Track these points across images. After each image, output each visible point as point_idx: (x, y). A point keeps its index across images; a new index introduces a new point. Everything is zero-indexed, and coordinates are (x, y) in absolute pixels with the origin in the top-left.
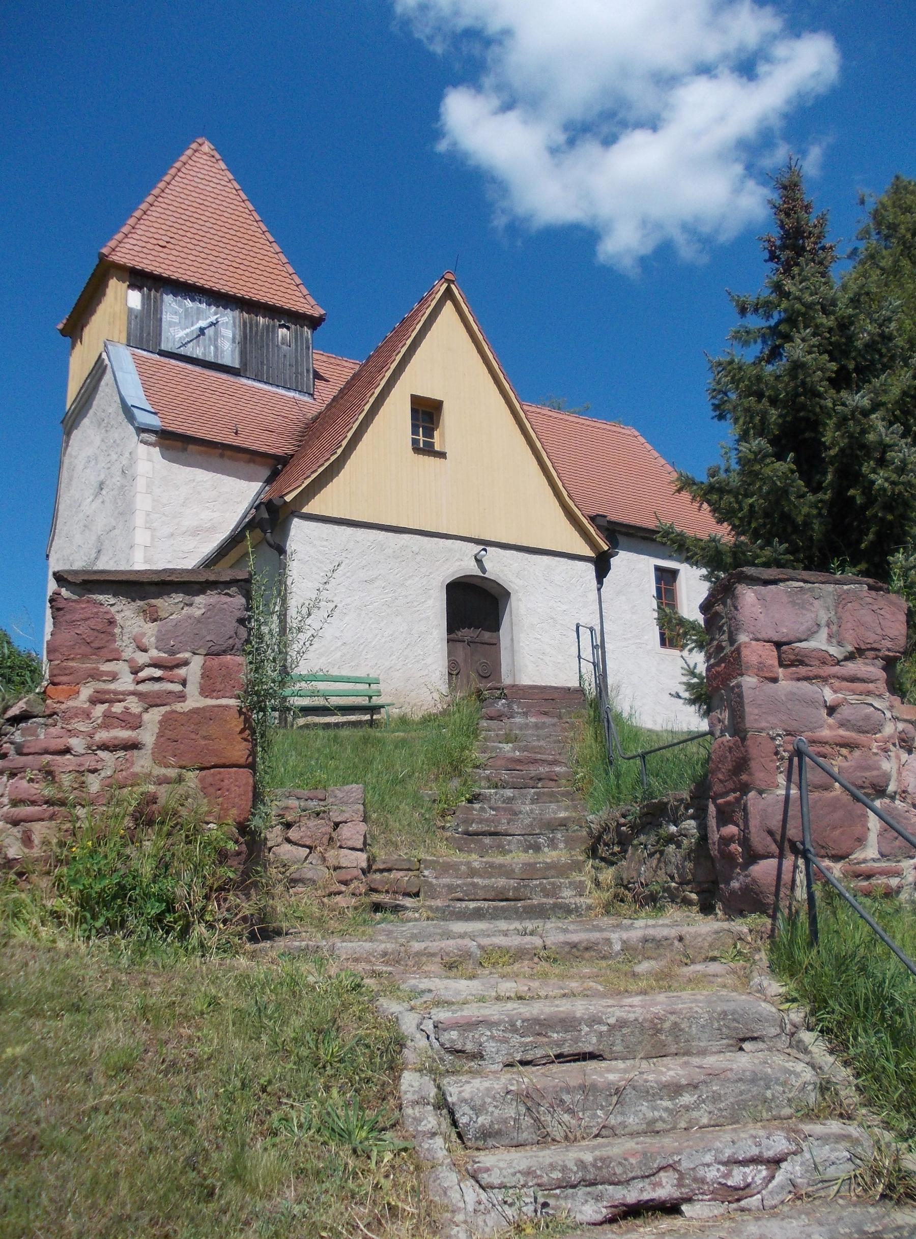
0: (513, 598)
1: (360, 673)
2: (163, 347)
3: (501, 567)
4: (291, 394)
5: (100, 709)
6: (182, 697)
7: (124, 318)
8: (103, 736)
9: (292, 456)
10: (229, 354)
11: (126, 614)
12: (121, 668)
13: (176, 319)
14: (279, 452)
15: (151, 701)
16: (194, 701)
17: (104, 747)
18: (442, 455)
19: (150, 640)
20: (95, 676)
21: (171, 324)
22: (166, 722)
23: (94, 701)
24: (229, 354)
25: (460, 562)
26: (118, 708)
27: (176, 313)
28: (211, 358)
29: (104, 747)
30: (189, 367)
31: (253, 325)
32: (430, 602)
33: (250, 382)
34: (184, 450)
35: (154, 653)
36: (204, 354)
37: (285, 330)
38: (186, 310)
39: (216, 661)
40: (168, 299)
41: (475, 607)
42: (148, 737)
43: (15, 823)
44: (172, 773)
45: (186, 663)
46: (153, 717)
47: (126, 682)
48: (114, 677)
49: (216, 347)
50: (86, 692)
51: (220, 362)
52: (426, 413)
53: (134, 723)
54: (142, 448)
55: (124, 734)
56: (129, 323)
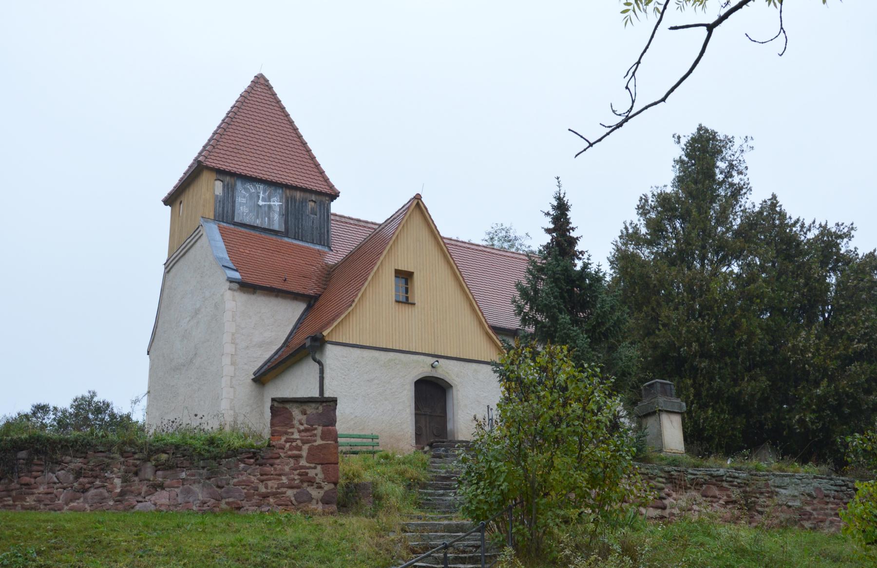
0: (454, 389)
1: (367, 432)
2: (236, 220)
3: (448, 371)
4: (318, 247)
5: (288, 445)
6: (315, 441)
7: (212, 201)
8: (290, 453)
9: (320, 295)
10: (277, 223)
11: (296, 412)
12: (295, 430)
13: (244, 201)
14: (311, 292)
15: (304, 442)
16: (319, 442)
17: (290, 457)
18: (414, 304)
19: (304, 421)
20: (286, 433)
21: (241, 204)
22: (310, 449)
23: (286, 441)
24: (277, 223)
25: (421, 368)
26: (294, 444)
27: (244, 197)
28: (266, 226)
29: (290, 457)
30: (253, 232)
31: (293, 199)
32: (405, 392)
33: (290, 240)
34: (254, 293)
35: (306, 426)
36: (261, 223)
37: (313, 204)
38: (251, 194)
39: (326, 428)
40: (239, 185)
41: (432, 394)
42: (304, 453)
43: (262, 481)
44: (313, 465)
45: (316, 429)
46: (306, 447)
47: (296, 436)
48: (293, 433)
49: (269, 218)
50: (284, 438)
51: (271, 228)
52: (405, 277)
53: (299, 448)
54: (229, 293)
55: (295, 452)
56: (215, 204)
